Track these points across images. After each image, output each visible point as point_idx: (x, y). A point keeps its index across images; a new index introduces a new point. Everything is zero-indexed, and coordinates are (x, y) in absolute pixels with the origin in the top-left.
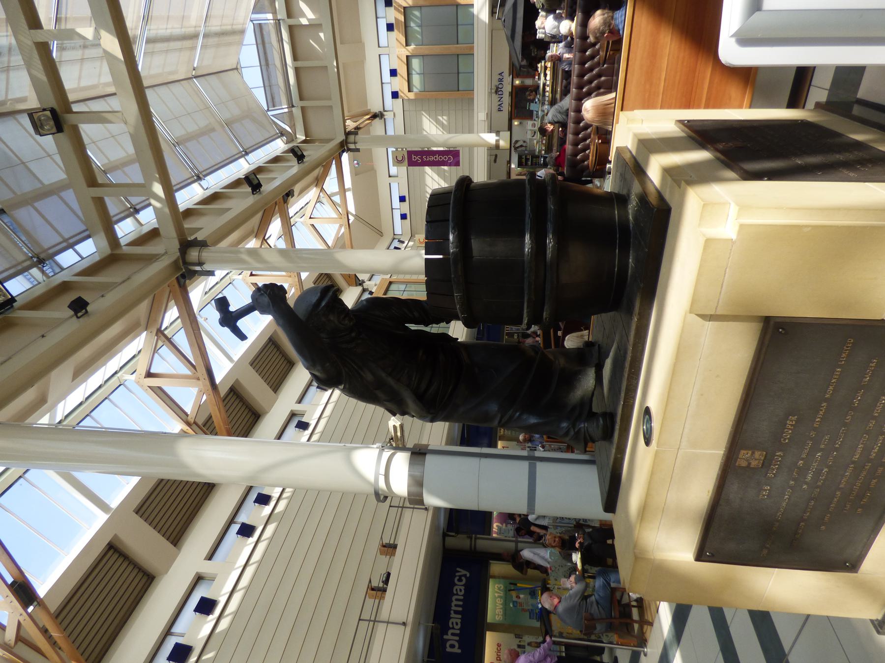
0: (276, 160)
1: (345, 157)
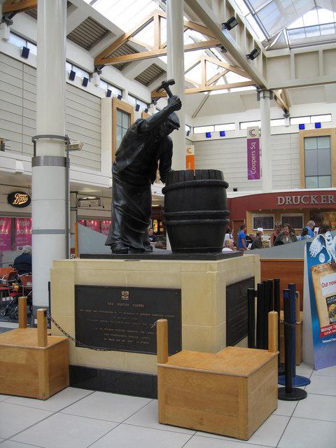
0: (249, 36)
1: (254, 88)
